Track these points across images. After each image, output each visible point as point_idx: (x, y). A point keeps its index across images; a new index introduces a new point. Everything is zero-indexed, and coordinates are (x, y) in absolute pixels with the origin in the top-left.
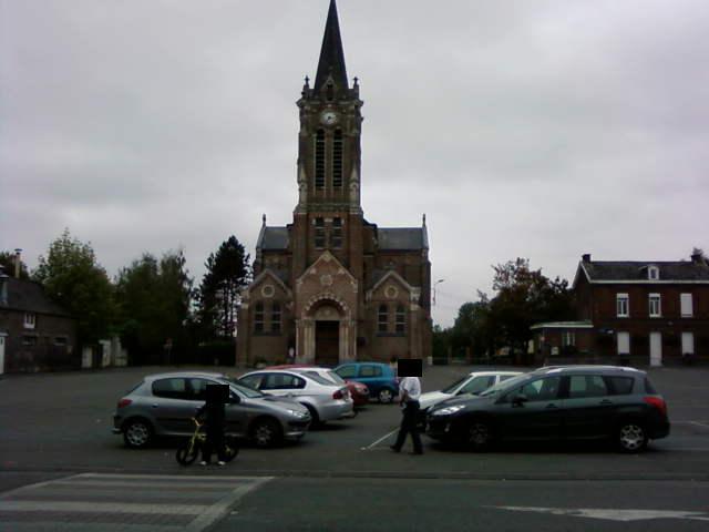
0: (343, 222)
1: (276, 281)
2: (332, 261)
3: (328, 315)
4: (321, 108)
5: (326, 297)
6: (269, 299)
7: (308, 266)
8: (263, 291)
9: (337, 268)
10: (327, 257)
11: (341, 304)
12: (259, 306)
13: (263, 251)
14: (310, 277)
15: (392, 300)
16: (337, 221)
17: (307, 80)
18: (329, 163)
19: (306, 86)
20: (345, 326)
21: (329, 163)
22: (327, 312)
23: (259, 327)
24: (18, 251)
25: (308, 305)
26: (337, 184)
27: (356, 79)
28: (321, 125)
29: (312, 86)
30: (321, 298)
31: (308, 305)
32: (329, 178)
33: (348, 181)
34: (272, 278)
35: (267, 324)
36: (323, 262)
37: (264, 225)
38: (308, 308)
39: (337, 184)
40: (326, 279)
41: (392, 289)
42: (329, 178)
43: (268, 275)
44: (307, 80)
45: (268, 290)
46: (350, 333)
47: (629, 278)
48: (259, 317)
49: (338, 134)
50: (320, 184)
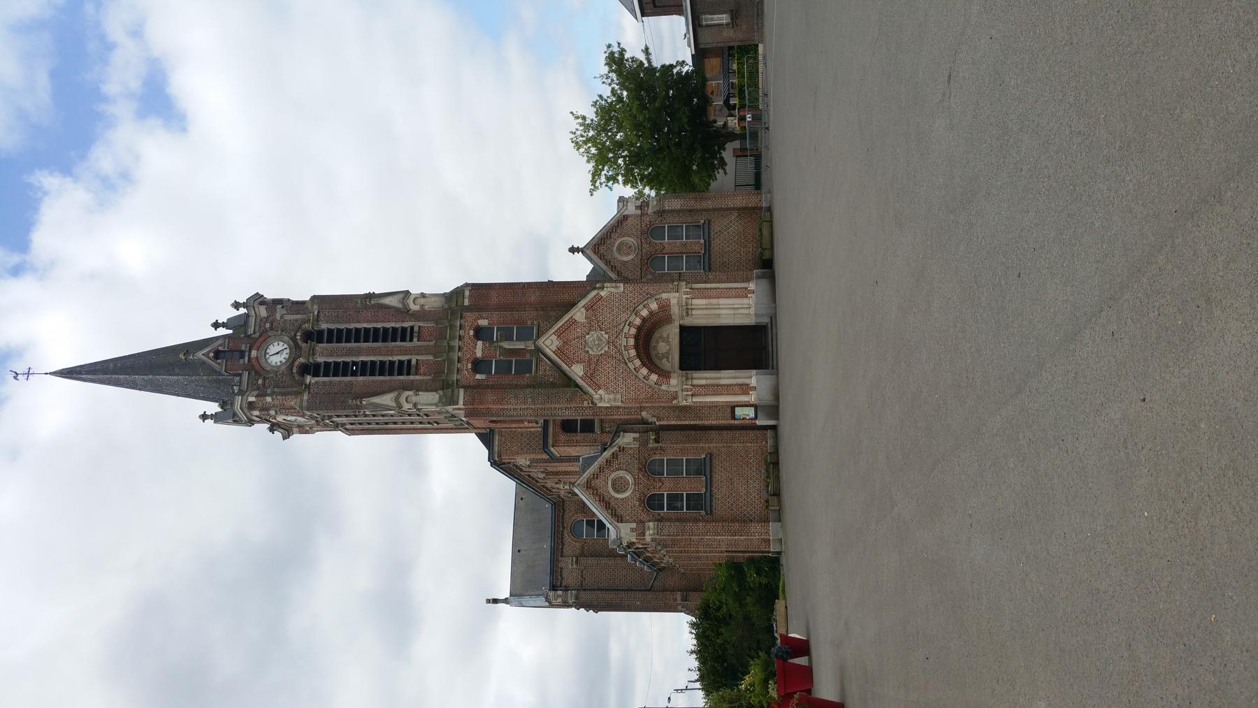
0: (483, 323)
1: (601, 469)
2: (559, 334)
3: (669, 343)
4: (257, 370)
5: (632, 342)
6: (637, 483)
7: (569, 382)
8: (629, 478)
9: (573, 322)
10: (549, 343)
11: (645, 313)
12: (652, 502)
13: (554, 588)
14: (590, 376)
15: (641, 248)
16: (480, 333)
17: (204, 417)
18: (367, 353)
19: (216, 418)
20: (688, 310)
21: (367, 353)
22: (662, 347)
23: (696, 502)
24: (204, 421)
25: (646, 378)
26: (404, 334)
27: (216, 325)
28: (291, 367)
29: (213, 408)
30: (633, 352)
31: (646, 378)
32: (394, 353)
33: (404, 312)
34: (595, 476)
35: (689, 486)
36: (559, 352)
37: (506, 601)
38: (654, 377)
39: (404, 334)
40: (596, 342)
41: (619, 249)
42: (394, 353)
43: (589, 486)
44: (204, 417)
45: (619, 486)
46: (704, 294)
47: (664, 466)
48: (674, 499)
49: (314, 336)
50: (404, 368)
